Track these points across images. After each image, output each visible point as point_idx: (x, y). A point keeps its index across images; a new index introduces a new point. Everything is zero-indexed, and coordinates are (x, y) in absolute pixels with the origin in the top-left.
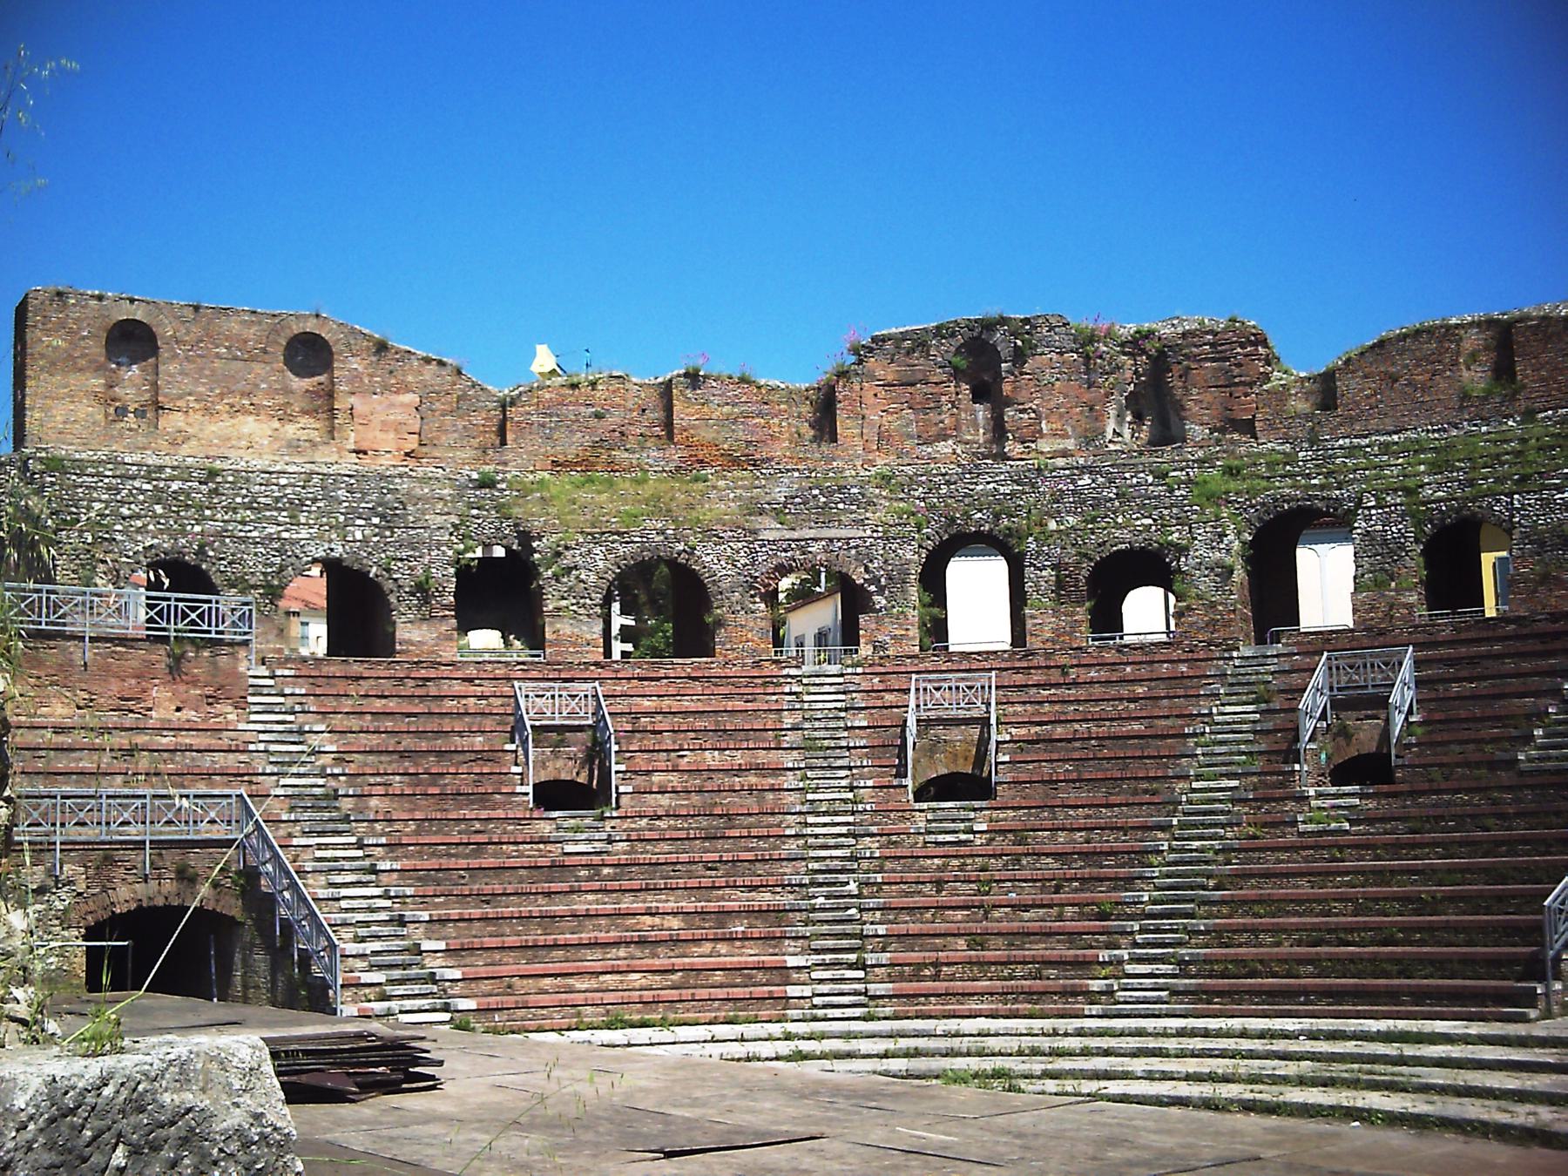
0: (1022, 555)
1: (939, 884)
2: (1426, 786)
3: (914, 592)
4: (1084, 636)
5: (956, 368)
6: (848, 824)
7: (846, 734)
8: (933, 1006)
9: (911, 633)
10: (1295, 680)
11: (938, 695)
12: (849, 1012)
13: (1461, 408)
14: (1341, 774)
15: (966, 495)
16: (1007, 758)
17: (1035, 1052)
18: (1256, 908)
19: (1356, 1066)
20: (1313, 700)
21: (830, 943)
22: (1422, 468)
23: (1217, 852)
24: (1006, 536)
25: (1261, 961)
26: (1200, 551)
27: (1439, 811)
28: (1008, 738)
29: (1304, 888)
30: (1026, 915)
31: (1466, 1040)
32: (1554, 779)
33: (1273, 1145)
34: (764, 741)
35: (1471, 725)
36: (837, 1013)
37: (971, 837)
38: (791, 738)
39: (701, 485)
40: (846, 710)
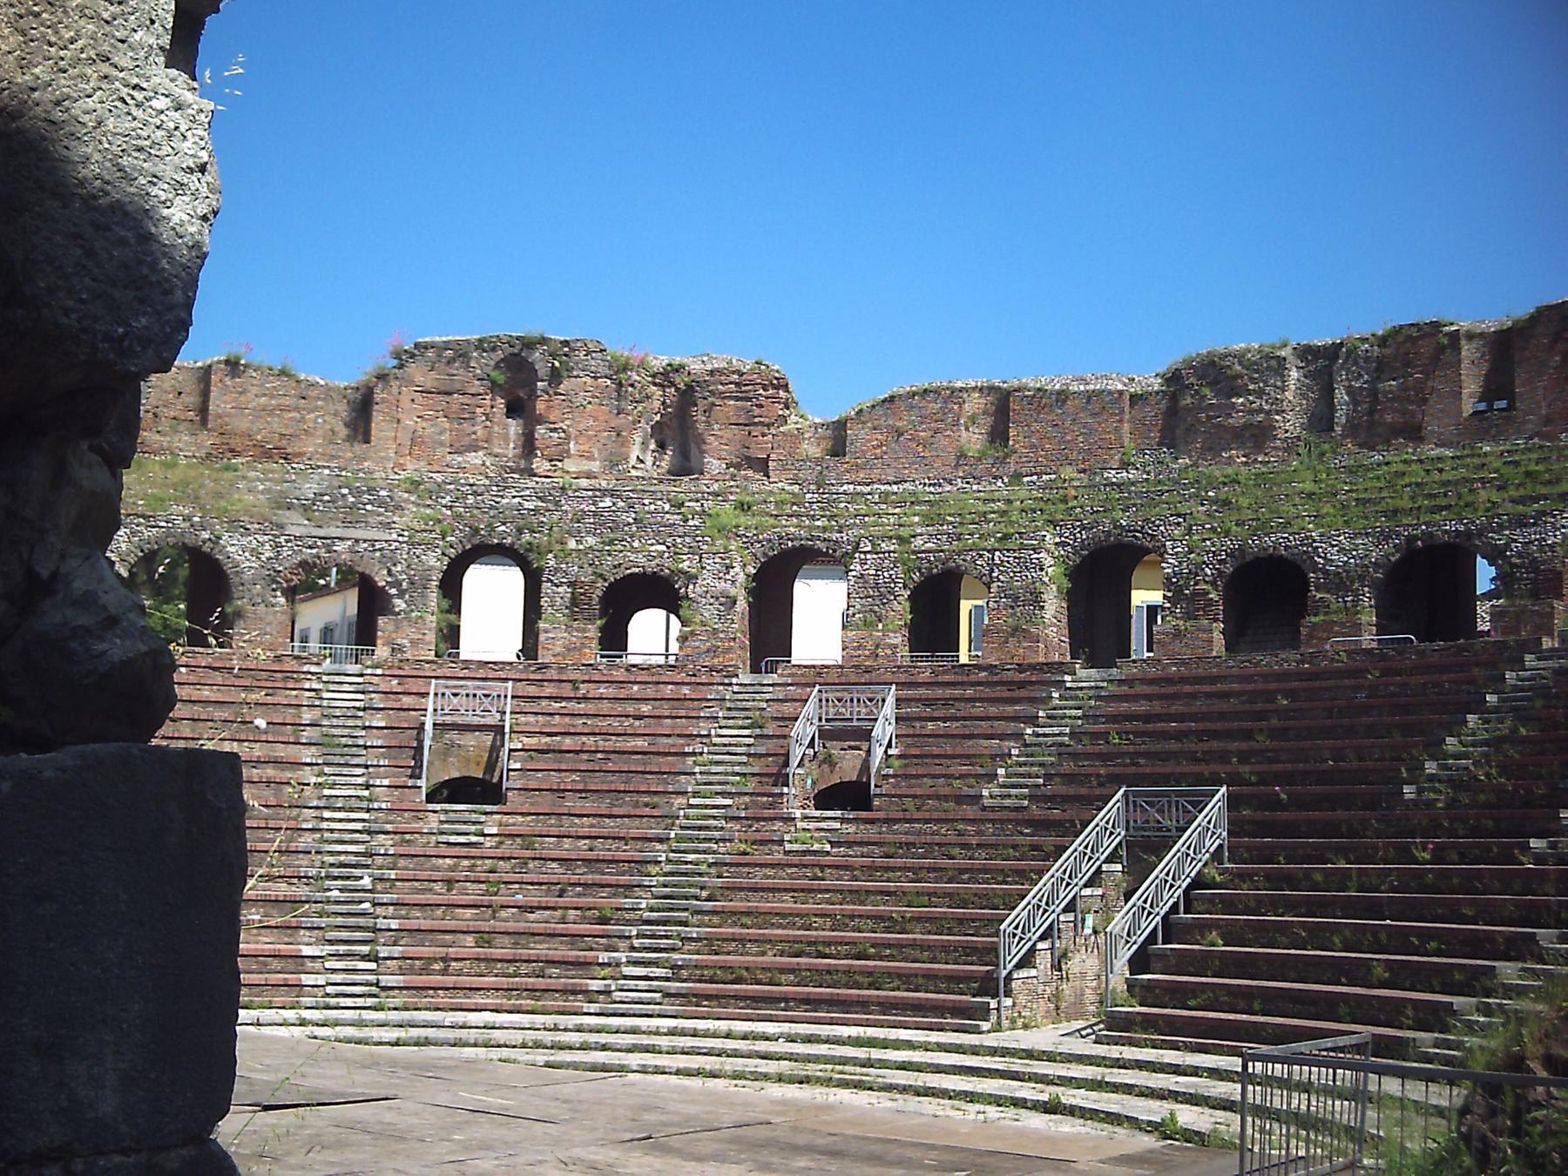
0: (540, 570)
1: (449, 882)
2: (900, 815)
3: (434, 597)
4: (593, 654)
5: (494, 382)
6: (364, 820)
7: (363, 733)
8: (442, 999)
9: (427, 638)
10: (788, 709)
11: (455, 700)
12: (360, 1002)
13: (957, 466)
14: (826, 798)
15: (492, 507)
16: (518, 766)
17: (538, 1045)
18: (744, 920)
19: (830, 1067)
20: (804, 729)
21: (344, 935)
22: (916, 519)
23: (710, 865)
24: (528, 550)
25: (747, 969)
26: (707, 580)
27: (911, 838)
28: (520, 746)
29: (787, 903)
30: (532, 916)
31: (926, 1047)
32: (1012, 815)
33: (782, 1113)
34: (283, 734)
35: (943, 761)
36: (349, 1002)
37: (481, 839)
38: (308, 734)
39: (230, 475)
40: (364, 709)
